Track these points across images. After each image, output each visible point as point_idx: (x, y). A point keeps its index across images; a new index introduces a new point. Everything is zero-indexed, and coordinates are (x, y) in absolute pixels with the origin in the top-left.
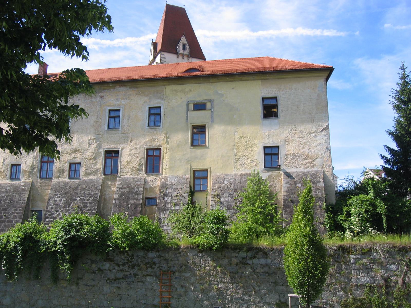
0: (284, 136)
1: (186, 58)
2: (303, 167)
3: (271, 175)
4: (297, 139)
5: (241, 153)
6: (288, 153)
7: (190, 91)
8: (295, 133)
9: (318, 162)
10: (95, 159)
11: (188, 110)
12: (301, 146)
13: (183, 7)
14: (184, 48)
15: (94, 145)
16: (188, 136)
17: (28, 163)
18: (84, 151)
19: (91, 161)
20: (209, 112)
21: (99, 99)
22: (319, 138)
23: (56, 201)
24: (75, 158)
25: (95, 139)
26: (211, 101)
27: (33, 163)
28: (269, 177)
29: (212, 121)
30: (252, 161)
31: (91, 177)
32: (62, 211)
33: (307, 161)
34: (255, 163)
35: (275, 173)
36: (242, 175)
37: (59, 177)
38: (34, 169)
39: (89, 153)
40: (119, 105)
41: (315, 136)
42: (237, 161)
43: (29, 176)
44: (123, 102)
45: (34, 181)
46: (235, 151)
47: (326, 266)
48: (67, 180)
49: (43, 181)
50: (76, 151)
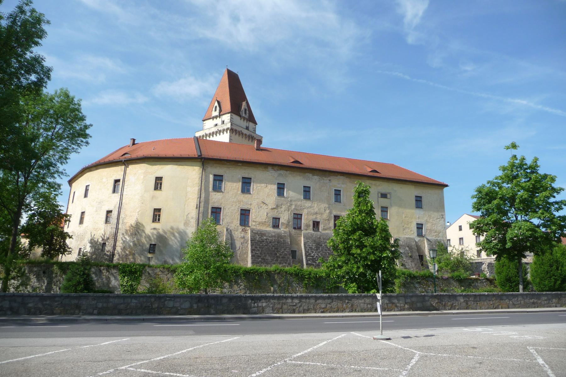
0: (425, 219)
1: (245, 121)
2: (434, 236)
3: (420, 240)
4: (431, 221)
5: (406, 226)
6: (428, 228)
7: (379, 185)
8: (430, 218)
9: (441, 234)
10: (328, 220)
11: (378, 197)
12: (433, 225)
13: (237, 73)
14: (245, 113)
15: (328, 211)
16: (240, 184)
17: (285, 218)
18: (322, 214)
19: (326, 221)
20: (389, 200)
21: (328, 181)
22: (441, 222)
23: (310, 245)
24: (316, 218)
25: (328, 207)
26: (389, 193)
27: (289, 218)
28: (419, 240)
29: (391, 206)
30: (411, 231)
31: (327, 232)
32: (315, 252)
33: (436, 233)
34: (412, 232)
35: (422, 239)
36: (407, 238)
37: (306, 230)
38: (289, 222)
39: (325, 216)
40: (340, 187)
41: (439, 221)
42: (404, 230)
43: (286, 227)
44: (343, 186)
45: (290, 231)
46: (403, 224)
47: (174, 300)
48: (312, 232)
49: (296, 231)
50: (316, 213)
